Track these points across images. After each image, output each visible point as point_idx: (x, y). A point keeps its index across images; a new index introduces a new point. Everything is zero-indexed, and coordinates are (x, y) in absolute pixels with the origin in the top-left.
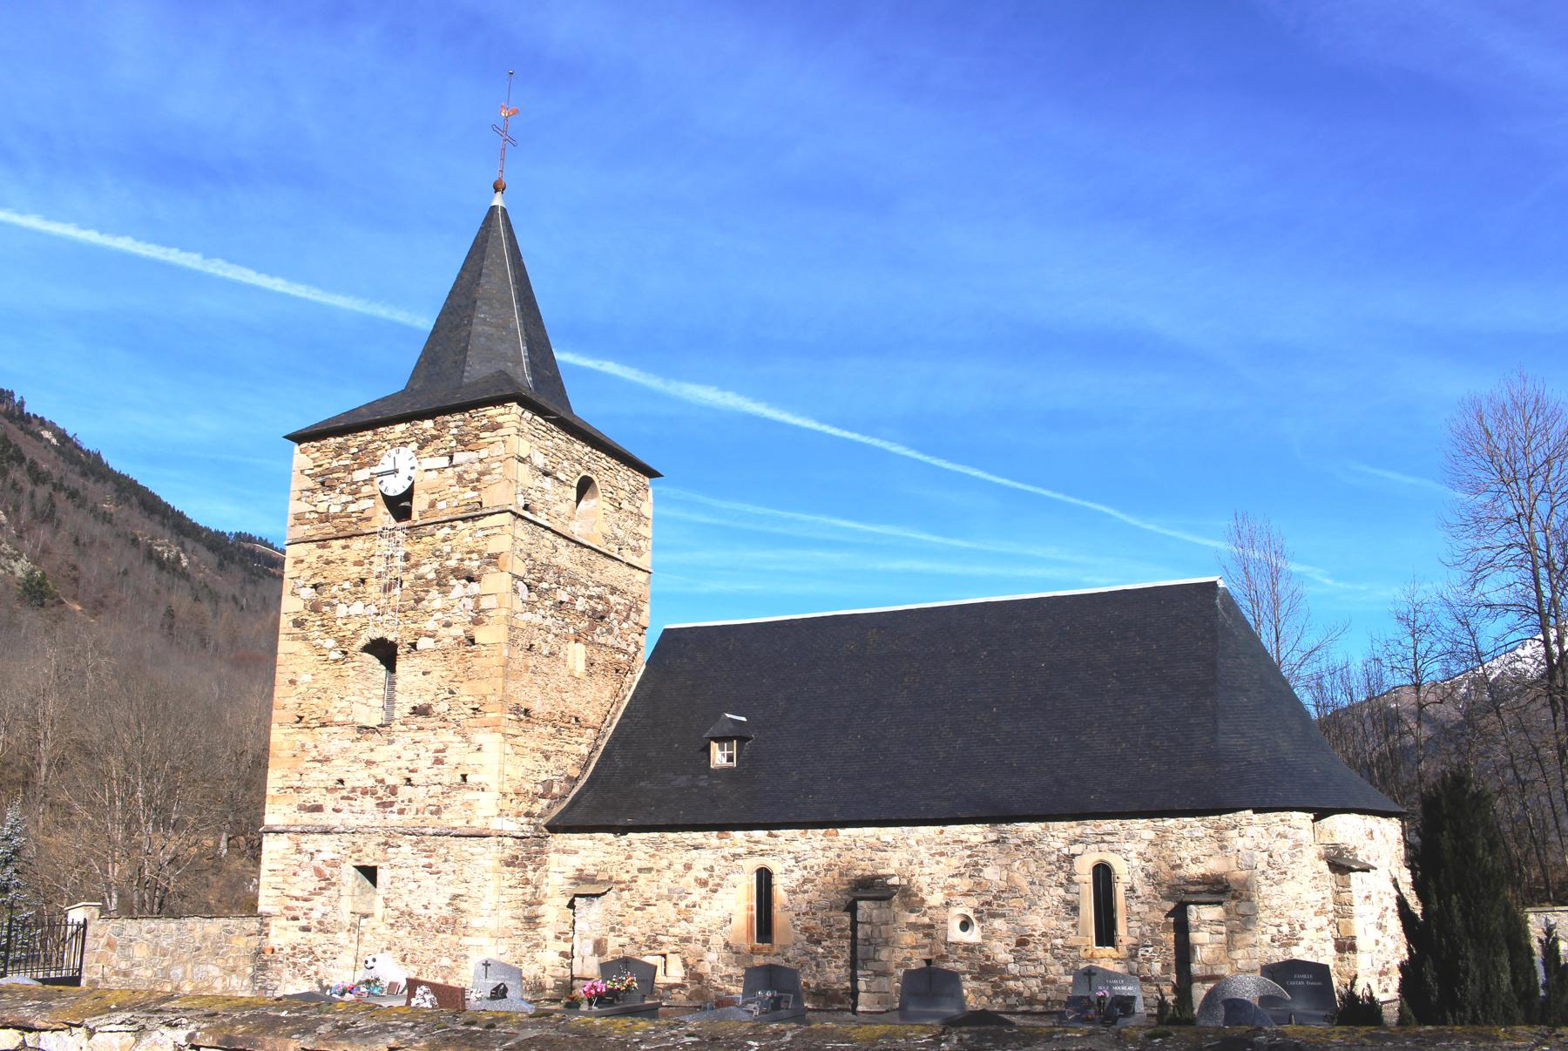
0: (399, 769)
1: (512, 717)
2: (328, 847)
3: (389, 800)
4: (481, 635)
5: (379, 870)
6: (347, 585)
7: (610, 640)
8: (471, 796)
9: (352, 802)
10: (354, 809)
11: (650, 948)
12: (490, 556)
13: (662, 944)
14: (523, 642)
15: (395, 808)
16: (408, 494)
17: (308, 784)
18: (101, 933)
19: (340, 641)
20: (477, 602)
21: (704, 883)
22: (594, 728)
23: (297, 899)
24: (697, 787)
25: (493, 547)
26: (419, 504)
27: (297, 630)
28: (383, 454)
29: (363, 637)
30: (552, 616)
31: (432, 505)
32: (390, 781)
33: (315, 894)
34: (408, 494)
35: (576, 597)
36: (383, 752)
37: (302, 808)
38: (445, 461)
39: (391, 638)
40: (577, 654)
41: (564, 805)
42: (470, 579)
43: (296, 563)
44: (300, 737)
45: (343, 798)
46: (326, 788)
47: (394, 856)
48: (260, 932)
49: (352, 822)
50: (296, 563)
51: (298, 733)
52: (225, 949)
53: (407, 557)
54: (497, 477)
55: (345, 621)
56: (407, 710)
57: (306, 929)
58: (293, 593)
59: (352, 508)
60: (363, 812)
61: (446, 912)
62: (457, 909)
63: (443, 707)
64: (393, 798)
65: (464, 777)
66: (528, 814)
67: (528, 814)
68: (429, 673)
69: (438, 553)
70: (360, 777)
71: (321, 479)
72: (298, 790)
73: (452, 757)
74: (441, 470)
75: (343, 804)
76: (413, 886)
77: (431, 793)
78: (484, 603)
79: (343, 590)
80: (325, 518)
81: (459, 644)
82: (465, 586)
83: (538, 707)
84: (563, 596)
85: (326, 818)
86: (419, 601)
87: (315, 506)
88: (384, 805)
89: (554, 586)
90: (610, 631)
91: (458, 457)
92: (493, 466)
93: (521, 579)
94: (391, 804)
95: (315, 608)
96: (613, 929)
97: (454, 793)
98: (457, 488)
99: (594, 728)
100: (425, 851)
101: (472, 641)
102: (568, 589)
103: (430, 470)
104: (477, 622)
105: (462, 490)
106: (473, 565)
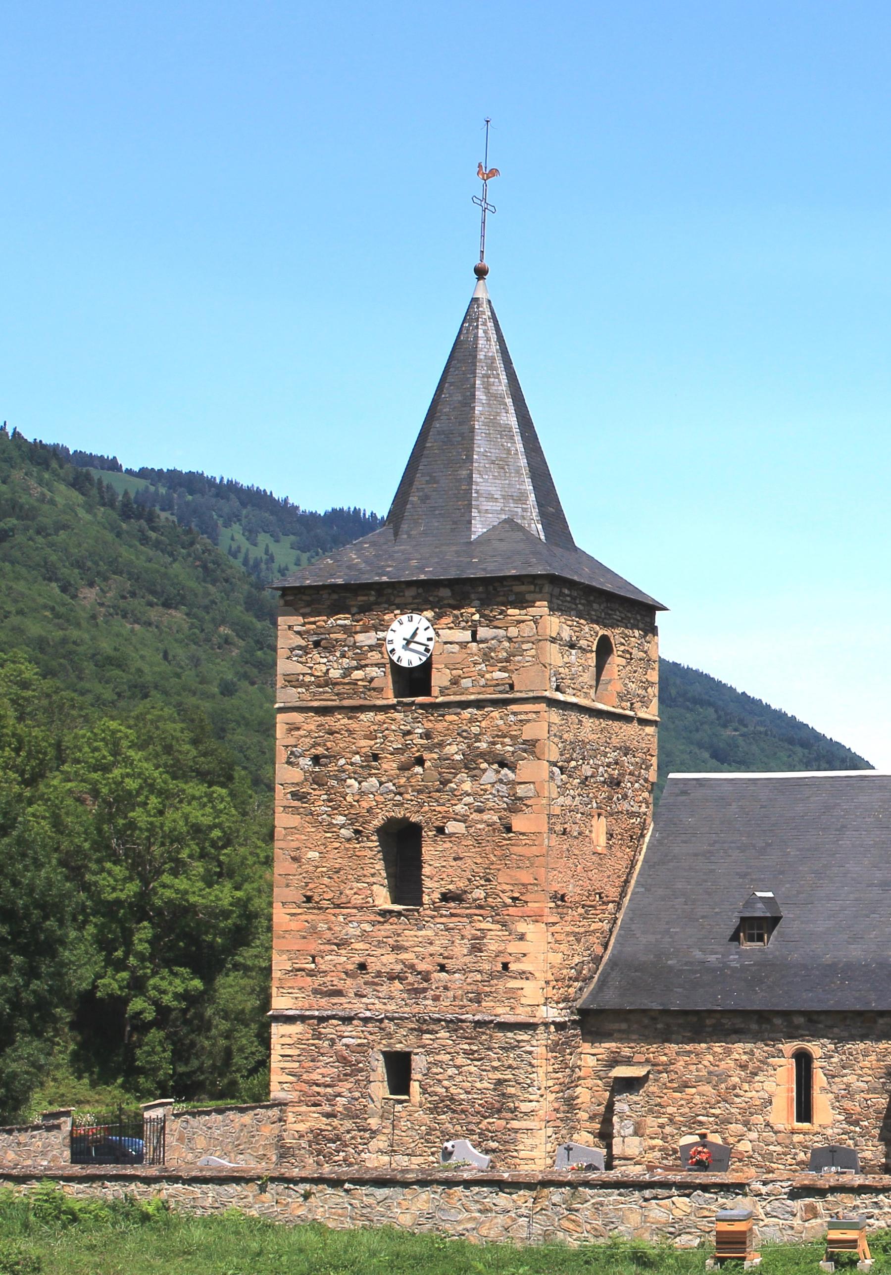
0: (431, 955)
1: (553, 905)
2: (352, 1035)
3: (421, 986)
4: (519, 823)
5: (413, 1057)
6: (357, 758)
7: (625, 806)
8: (513, 984)
9: (378, 988)
10: (380, 995)
11: (690, 1128)
12: (525, 742)
13: (701, 1123)
14: (558, 828)
15: (430, 993)
16: (426, 668)
17: (323, 967)
18: (174, 1128)
19: (352, 820)
20: (513, 788)
21: (743, 1067)
22: (613, 902)
23: (318, 1085)
24: (729, 967)
25: (529, 732)
26: (439, 679)
27: (297, 803)
28: (392, 620)
29: (380, 816)
30: (579, 795)
31: (455, 682)
32: (422, 966)
33: (340, 1081)
34: (426, 668)
35: (597, 767)
36: (410, 936)
37: (316, 992)
38: (467, 635)
39: (414, 819)
40: (599, 828)
41: (592, 986)
42: (502, 765)
43: (290, 730)
44: (310, 917)
45: (365, 984)
46: (346, 973)
47: (431, 1042)
48: (280, 1120)
49: (379, 1008)
50: (290, 730)
51: (305, 913)
52: (257, 1138)
53: (427, 735)
54: (528, 658)
55: (357, 798)
56: (436, 896)
57: (328, 1115)
58: (289, 763)
59: (358, 674)
60: (391, 998)
61: (491, 1097)
62: (504, 1094)
63: (479, 893)
64: (425, 985)
65: (505, 966)
66: (566, 1000)
67: (566, 1000)
68: (461, 859)
69: (464, 734)
70: (386, 961)
71: (315, 638)
72: (311, 974)
73: (493, 946)
74: (463, 645)
75: (367, 990)
76: (451, 1071)
77: (469, 980)
78: (520, 791)
79: (352, 764)
80: (326, 682)
81: (494, 830)
82: (498, 772)
83: (572, 891)
84: (587, 770)
85: (349, 1005)
86: (445, 783)
87: (311, 668)
88: (416, 992)
89: (581, 762)
90: (625, 797)
91: (483, 632)
92: (525, 647)
93: (555, 764)
94: (425, 990)
95: (318, 781)
96: (651, 1111)
97: (495, 981)
98: (483, 666)
99: (613, 902)
100: (467, 1038)
101: (509, 829)
102: (591, 762)
103: (451, 643)
104: (513, 809)
105: (490, 669)
106: (506, 748)
